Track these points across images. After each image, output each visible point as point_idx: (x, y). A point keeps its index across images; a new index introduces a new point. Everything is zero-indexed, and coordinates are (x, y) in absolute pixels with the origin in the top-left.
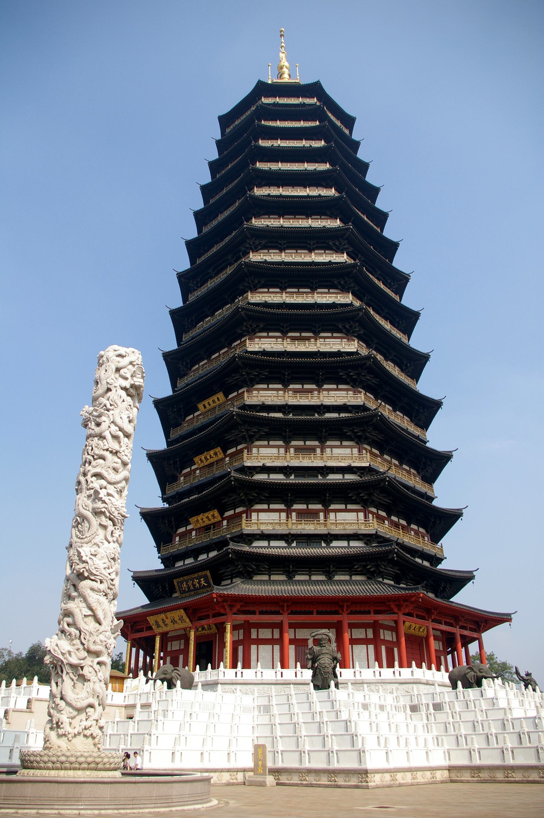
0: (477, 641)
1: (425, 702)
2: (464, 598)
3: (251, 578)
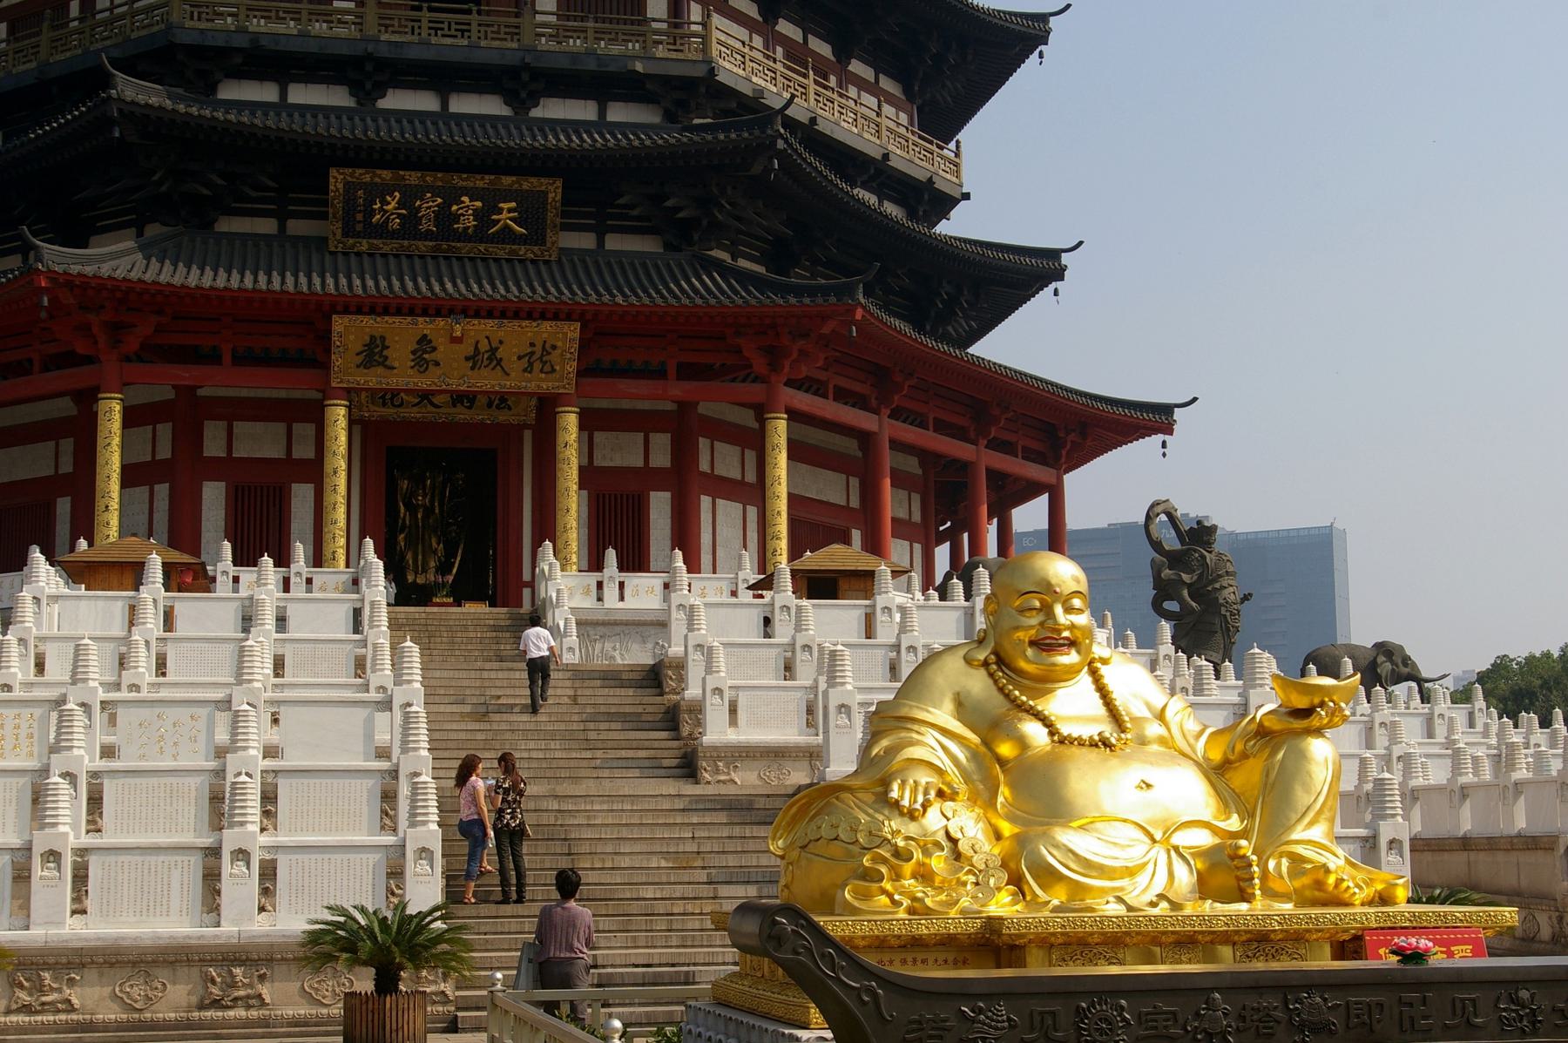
0: (1046, 497)
2: (1019, 344)
3: (208, 225)
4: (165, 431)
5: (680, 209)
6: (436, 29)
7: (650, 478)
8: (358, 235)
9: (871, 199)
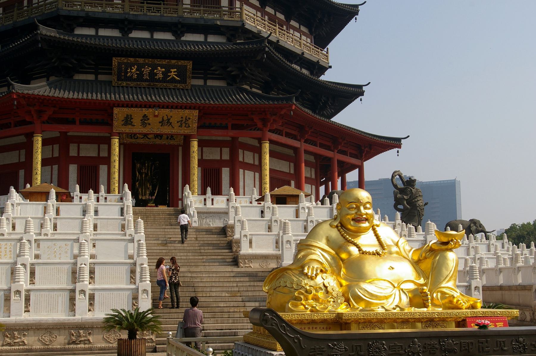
0: (357, 169)
1: (315, 219)
2: (348, 117)
3: (71, 77)
4: (56, 147)
5: (233, 71)
6: (149, 10)
7: (222, 163)
8: (122, 80)
9: (298, 68)
